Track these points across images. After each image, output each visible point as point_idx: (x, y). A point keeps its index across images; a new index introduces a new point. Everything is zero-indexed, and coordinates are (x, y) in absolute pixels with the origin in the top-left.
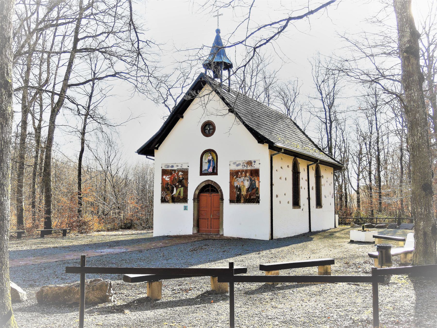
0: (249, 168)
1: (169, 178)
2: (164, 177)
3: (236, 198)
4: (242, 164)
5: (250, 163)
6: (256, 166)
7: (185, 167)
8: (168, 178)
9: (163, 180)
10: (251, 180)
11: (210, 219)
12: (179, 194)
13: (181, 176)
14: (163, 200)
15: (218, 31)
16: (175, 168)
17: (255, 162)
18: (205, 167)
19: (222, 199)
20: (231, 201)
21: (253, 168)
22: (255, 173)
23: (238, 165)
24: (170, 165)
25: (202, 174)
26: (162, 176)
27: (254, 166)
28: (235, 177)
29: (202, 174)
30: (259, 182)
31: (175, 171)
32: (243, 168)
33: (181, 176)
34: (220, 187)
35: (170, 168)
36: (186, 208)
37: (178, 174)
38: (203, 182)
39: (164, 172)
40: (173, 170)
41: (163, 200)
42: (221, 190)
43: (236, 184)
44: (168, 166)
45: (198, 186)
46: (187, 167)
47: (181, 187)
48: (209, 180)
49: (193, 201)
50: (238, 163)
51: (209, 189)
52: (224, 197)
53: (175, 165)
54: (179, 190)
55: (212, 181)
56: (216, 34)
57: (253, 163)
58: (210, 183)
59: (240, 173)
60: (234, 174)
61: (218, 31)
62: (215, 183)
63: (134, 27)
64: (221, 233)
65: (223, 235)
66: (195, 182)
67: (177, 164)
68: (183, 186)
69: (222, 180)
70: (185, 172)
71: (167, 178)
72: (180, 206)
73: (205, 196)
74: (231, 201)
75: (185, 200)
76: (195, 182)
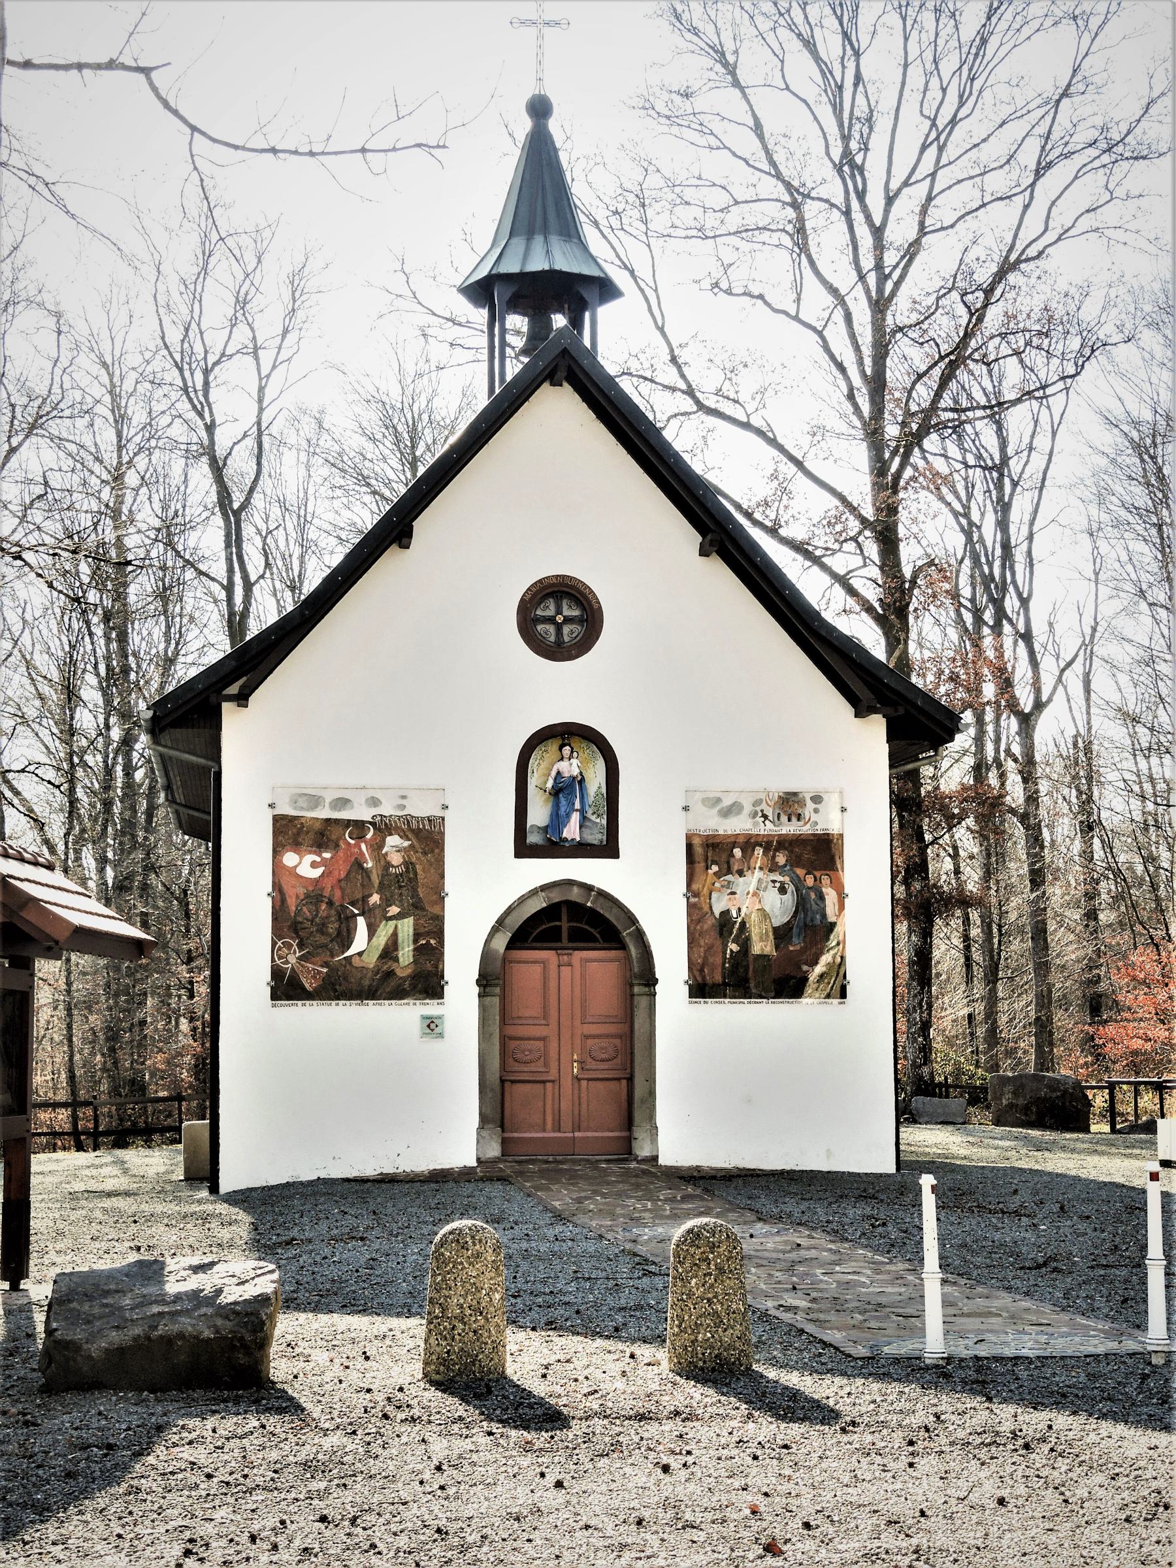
0: (789, 828)
1: (324, 862)
2: (290, 859)
3: (734, 971)
4: (748, 808)
5: (790, 803)
6: (828, 821)
7: (421, 808)
8: (314, 865)
9: (278, 868)
10: (798, 884)
11: (567, 1083)
12: (390, 952)
13: (396, 859)
14: (285, 987)
15: (540, 109)
16: (363, 813)
17: (817, 799)
18: (538, 814)
19: (650, 981)
20: (700, 990)
21: (806, 829)
22: (821, 854)
23: (727, 813)
24: (329, 797)
25: (523, 849)
26: (277, 851)
27: (814, 817)
28: (715, 868)
29: (523, 849)
30: (842, 897)
31: (359, 827)
32: (756, 824)
33: (396, 859)
34: (632, 920)
35: (324, 813)
36: (431, 1025)
37: (382, 845)
38: (534, 893)
39: (288, 832)
40: (348, 823)
41: (285, 987)
42: (640, 936)
43: (720, 904)
44: (316, 801)
45: (510, 910)
46: (440, 813)
47: (399, 916)
48: (570, 883)
49: (476, 990)
50: (727, 801)
51: (576, 924)
52: (661, 970)
53: (359, 799)
54: (384, 932)
55: (588, 888)
56: (524, 125)
57: (810, 805)
58: (575, 895)
59: (737, 852)
60: (709, 856)
61: (540, 109)
62: (602, 894)
63: (1046, 143)
64: (643, 1151)
65: (655, 1158)
66: (485, 886)
67: (371, 793)
68: (416, 907)
69: (647, 884)
70: (428, 838)
71: (306, 866)
72: (405, 1015)
73: (535, 965)
74: (700, 990)
75: (428, 983)
76: (485, 886)
